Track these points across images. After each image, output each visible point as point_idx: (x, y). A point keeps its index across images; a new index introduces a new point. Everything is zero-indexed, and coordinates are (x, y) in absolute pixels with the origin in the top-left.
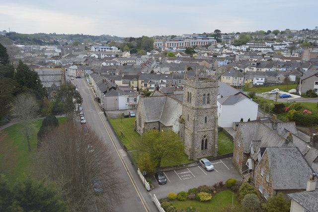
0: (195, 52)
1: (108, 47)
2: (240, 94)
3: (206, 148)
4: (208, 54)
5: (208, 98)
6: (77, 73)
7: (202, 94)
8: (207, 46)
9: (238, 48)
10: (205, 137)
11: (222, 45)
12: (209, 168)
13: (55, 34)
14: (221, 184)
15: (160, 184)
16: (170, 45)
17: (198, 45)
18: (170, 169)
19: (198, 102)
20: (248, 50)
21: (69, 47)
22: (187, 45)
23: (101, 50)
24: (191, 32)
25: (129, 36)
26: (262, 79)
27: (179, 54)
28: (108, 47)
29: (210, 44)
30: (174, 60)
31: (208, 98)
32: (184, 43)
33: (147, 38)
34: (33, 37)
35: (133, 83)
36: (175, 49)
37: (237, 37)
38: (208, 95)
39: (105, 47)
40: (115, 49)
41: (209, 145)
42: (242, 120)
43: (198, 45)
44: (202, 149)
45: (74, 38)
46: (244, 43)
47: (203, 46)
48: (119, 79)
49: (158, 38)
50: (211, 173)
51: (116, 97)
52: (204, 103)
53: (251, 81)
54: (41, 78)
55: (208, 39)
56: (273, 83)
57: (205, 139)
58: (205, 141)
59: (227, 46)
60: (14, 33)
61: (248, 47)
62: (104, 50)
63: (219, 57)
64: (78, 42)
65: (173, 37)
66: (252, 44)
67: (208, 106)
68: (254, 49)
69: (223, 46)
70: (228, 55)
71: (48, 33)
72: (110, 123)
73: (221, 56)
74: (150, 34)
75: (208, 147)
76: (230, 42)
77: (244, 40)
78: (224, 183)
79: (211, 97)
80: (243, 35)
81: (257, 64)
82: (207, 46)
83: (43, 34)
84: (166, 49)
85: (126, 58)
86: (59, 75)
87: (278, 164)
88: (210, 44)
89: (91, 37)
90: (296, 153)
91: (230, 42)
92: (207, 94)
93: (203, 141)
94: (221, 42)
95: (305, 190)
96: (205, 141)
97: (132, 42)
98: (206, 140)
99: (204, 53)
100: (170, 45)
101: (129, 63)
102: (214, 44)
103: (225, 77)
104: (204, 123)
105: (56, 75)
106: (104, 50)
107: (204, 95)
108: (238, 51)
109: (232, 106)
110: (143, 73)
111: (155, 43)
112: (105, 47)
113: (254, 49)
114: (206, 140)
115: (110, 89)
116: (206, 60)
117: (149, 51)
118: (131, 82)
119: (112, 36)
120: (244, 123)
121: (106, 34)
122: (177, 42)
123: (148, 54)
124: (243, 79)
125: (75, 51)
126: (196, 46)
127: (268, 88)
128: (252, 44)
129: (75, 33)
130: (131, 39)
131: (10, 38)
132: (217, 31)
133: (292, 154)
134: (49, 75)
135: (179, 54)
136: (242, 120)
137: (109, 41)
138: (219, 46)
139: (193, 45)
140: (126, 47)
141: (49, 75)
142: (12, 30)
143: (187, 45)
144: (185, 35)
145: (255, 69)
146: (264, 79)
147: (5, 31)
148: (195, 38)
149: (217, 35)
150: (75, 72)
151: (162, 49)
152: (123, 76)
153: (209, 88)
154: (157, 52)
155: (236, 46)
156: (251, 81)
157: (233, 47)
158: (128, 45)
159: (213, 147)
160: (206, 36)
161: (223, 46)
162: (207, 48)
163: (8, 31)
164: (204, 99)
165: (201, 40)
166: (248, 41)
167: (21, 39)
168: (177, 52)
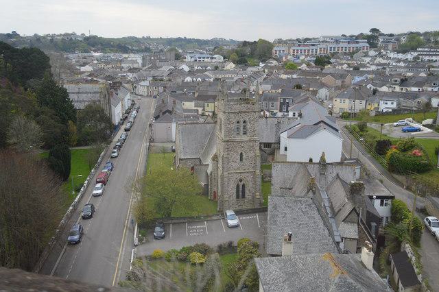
0: (330, 63)
1: (209, 56)
2: (322, 124)
3: (243, 196)
4: (348, 64)
5: (245, 127)
6: (148, 90)
7: (235, 121)
8: (352, 54)
9: (400, 56)
10: (241, 181)
11: (376, 51)
12: (231, 222)
13: (149, 38)
14: (230, 244)
15: (156, 238)
16: (297, 52)
17: (340, 51)
18: (181, 221)
19: (229, 132)
20: (416, 58)
21: (154, 56)
22: (322, 52)
23: (198, 59)
24: (337, 33)
25: (242, 39)
26: (392, 104)
27: (304, 65)
28: (209, 56)
29: (358, 50)
30: (293, 73)
31: (245, 127)
32: (318, 50)
33: (264, 41)
34: (118, 42)
35: (208, 106)
36: (302, 58)
37: (403, 40)
38: (244, 122)
39: (203, 56)
40: (219, 58)
41: (247, 193)
42: (311, 160)
43: (340, 51)
44: (238, 197)
45: (173, 44)
46: (414, 49)
47: (345, 54)
48: (190, 100)
49: (280, 42)
50: (234, 231)
51: (169, 124)
52: (238, 134)
53: (376, 106)
54: (72, 97)
55: (357, 43)
56: (407, 110)
57: (241, 184)
58: (241, 189)
59: (384, 53)
60: (95, 37)
61: (416, 54)
62: (202, 59)
63: (365, 69)
64: (176, 48)
65: (307, 40)
66: (426, 49)
67: (245, 138)
68: (427, 58)
69: (377, 53)
70: (379, 67)
71: (139, 36)
72: (148, 156)
73: (368, 69)
74: (271, 39)
75: (246, 195)
76: (390, 47)
77: (414, 43)
78: (235, 244)
79: (249, 126)
80: (412, 36)
81: (402, 80)
82: (352, 54)
83: (133, 38)
84: (289, 57)
85: (228, 72)
86: (97, 93)
87: (279, 219)
88: (358, 50)
89: (198, 41)
90: (310, 206)
91: (390, 47)
92: (242, 121)
93: (238, 186)
94: (376, 47)
95: (281, 256)
96: (241, 187)
97: (245, 48)
98: (243, 186)
99: (342, 64)
100: (297, 52)
101: (228, 78)
102: (365, 50)
103: (338, 100)
104: (238, 161)
105: (95, 93)
106: (202, 59)
107: (238, 122)
108: (399, 61)
109: (304, 140)
110: (233, 92)
111: (275, 49)
112: (203, 56)
113: (427, 58)
114: (243, 186)
115: (164, 113)
116: (332, 75)
117: (263, 61)
118: (206, 104)
119: (228, 39)
120: (314, 163)
121: (219, 37)
122: (307, 48)
123: (262, 65)
124: (364, 102)
125: (161, 60)
126: (337, 53)
127: (396, 117)
128: (426, 49)
129: (175, 36)
130: (245, 44)
131: (88, 44)
132: (373, 30)
133: (303, 207)
134: (86, 93)
135: (304, 65)
136: (311, 160)
137: (216, 46)
138: (372, 53)
139: (332, 51)
140: (234, 56)
141: (86, 93)
142: (93, 34)
143: (322, 52)
144: (324, 37)
145: (398, 89)
146: (395, 103)
147: (83, 34)
148: (337, 42)
149: (373, 38)
150: (146, 90)
151: (284, 58)
152: (196, 95)
153: (245, 112)
154: (275, 63)
155: (398, 52)
156: (376, 106)
157: (392, 55)
158: (237, 52)
159: (254, 196)
160: (353, 39)
161: (377, 53)
162: (352, 57)
163: (87, 35)
164: (238, 128)
165: (346, 45)
166: (420, 45)
167: (102, 45)
168: (303, 62)
